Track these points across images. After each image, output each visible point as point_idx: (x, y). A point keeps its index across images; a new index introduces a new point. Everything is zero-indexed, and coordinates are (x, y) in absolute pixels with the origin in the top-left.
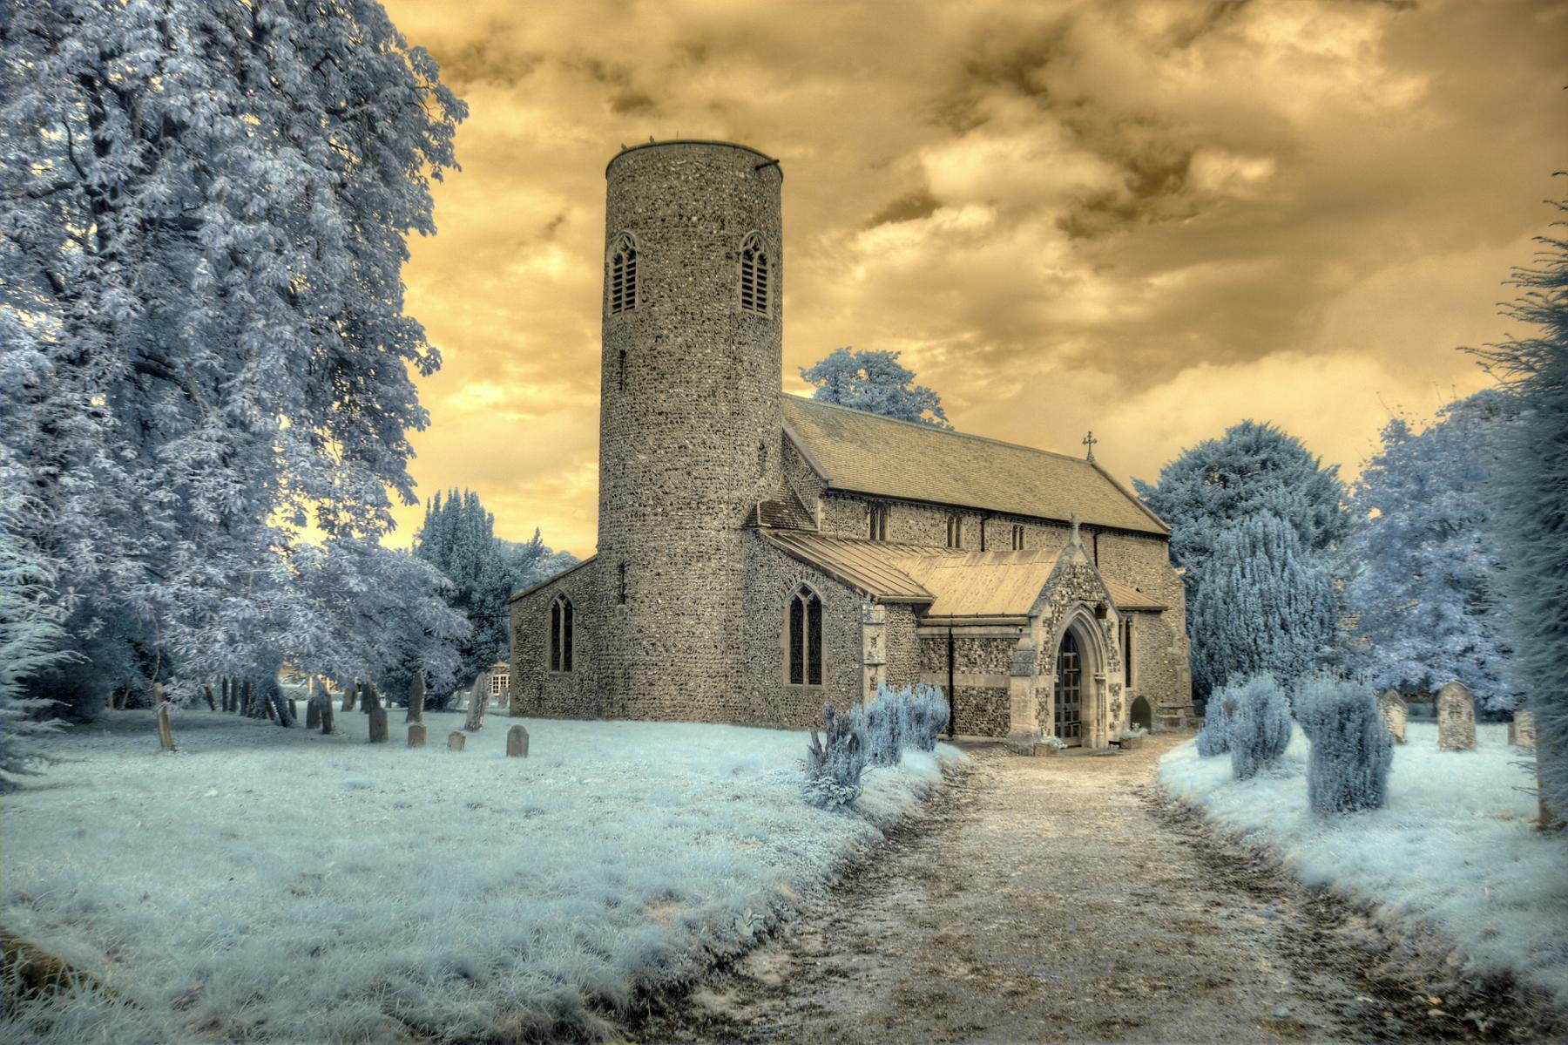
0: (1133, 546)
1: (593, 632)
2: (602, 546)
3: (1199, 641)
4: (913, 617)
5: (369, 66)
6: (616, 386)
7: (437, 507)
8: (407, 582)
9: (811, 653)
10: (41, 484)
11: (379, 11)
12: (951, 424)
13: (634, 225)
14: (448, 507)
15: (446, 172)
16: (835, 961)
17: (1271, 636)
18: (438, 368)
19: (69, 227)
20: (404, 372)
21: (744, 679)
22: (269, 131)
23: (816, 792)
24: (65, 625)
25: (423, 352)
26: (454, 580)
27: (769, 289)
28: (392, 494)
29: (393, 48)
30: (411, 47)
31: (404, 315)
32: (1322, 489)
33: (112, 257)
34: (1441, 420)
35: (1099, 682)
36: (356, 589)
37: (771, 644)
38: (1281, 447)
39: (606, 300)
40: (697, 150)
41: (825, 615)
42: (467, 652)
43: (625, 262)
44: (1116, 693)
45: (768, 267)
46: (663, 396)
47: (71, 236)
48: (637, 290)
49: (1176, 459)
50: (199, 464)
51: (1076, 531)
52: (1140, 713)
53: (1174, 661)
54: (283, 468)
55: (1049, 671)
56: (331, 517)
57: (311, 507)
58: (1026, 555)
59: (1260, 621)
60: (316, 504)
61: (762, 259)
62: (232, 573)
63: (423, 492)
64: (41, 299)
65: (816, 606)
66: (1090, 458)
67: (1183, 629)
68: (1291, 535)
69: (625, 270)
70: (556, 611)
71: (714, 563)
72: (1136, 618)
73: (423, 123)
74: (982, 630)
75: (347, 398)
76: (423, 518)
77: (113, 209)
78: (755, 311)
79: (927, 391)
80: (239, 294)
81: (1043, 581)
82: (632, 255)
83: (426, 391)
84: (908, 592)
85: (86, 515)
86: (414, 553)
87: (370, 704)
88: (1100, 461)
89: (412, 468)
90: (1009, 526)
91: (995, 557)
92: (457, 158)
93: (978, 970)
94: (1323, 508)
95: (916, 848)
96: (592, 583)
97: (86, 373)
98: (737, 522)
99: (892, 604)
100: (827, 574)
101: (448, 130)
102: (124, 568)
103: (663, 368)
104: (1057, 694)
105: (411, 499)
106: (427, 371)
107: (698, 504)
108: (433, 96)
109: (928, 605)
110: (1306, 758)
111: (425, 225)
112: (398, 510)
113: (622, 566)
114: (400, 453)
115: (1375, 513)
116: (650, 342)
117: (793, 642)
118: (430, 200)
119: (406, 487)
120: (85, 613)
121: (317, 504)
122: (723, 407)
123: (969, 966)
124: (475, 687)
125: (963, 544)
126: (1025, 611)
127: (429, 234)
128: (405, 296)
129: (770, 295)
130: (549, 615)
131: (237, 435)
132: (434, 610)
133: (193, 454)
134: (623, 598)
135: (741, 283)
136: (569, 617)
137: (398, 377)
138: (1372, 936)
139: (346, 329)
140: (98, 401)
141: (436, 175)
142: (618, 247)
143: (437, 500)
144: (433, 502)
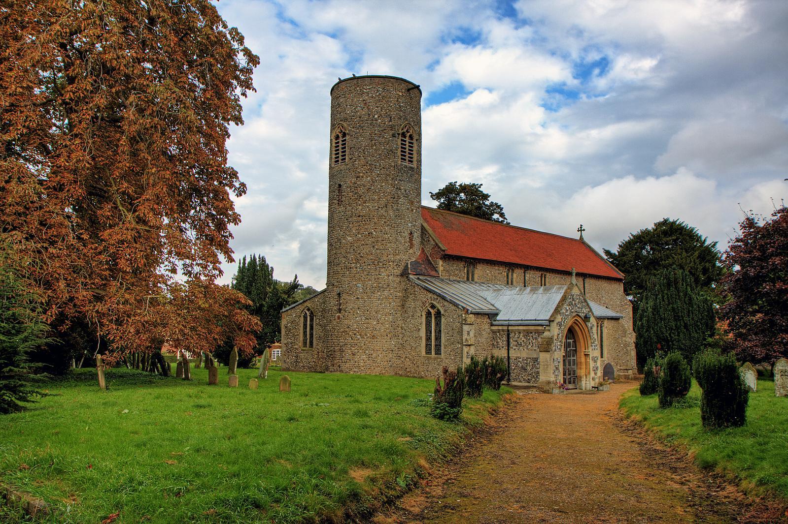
0: (604, 285)
1: (324, 327)
2: (329, 283)
3: (640, 334)
4: (488, 321)
5: (208, 38)
6: (336, 202)
7: (244, 263)
8: (232, 303)
9: (436, 339)
10: (39, 252)
11: (213, 9)
12: (508, 221)
13: (346, 120)
14: (250, 263)
15: (249, 92)
16: (449, 501)
17: (679, 333)
18: (245, 193)
19: (53, 121)
20: (228, 194)
21: (401, 352)
22: (157, 71)
23: (438, 411)
24: (50, 325)
25: (237, 185)
26: (253, 301)
27: (414, 152)
28: (221, 257)
29: (221, 28)
30: (230, 27)
31: (227, 166)
32: (707, 254)
33: (76, 135)
34: (775, 218)
35: (587, 355)
36: (203, 306)
37: (415, 334)
38: (683, 232)
39: (331, 158)
40: (377, 80)
41: (443, 320)
42: (258, 338)
43: (341, 139)
44: (595, 362)
45: (414, 141)
46: (360, 207)
47: (55, 125)
48: (347, 153)
49: (627, 239)
50: (122, 242)
51: (574, 277)
52: (608, 371)
53: (626, 345)
54: (165, 243)
55: (560, 349)
56: (190, 269)
57: (179, 264)
58: (546, 290)
59: (673, 324)
60: (182, 262)
61: (411, 137)
62: (138, 298)
63: (237, 256)
64: (39, 158)
65: (438, 314)
67: (631, 328)
68: (690, 279)
69: (341, 143)
70: (305, 317)
72: (606, 322)
73: (236, 67)
74: (525, 328)
75: (198, 208)
76: (237, 269)
77: (76, 112)
78: (406, 164)
79: (496, 204)
80: (142, 155)
81: (557, 302)
82: (344, 135)
83: (239, 203)
84: (486, 308)
85: (62, 268)
86: (232, 287)
87: (209, 364)
88: (586, 239)
89: (231, 244)
90: (539, 274)
91: (531, 290)
92: (254, 85)
93: (524, 507)
94: (707, 265)
95: (490, 441)
96: (324, 303)
97: (61, 195)
98: (398, 271)
99: (477, 314)
100: (444, 298)
101: (249, 71)
102: (83, 294)
103: (360, 193)
104: (564, 360)
105: (231, 260)
106: (239, 195)
107: (377, 262)
108: (241, 54)
109: (497, 314)
110: (700, 398)
111: (238, 120)
112: (224, 264)
113: (339, 294)
114: (225, 236)
115: (737, 268)
116: (354, 180)
117: (427, 333)
118: (240, 107)
119: (228, 252)
120: (61, 318)
121: (183, 262)
122: (391, 213)
123: (519, 505)
124: (263, 356)
125: (515, 283)
126: (548, 318)
127: (240, 125)
128: (228, 156)
129: (415, 156)
130: (302, 319)
131: (140, 227)
132: (242, 316)
133: (119, 237)
134: (340, 310)
135: (400, 149)
136: (312, 320)
137: (225, 198)
138: (740, 497)
139: (198, 173)
140: (69, 210)
141: (244, 94)
142: (337, 131)
143: (244, 259)
144: (242, 261)
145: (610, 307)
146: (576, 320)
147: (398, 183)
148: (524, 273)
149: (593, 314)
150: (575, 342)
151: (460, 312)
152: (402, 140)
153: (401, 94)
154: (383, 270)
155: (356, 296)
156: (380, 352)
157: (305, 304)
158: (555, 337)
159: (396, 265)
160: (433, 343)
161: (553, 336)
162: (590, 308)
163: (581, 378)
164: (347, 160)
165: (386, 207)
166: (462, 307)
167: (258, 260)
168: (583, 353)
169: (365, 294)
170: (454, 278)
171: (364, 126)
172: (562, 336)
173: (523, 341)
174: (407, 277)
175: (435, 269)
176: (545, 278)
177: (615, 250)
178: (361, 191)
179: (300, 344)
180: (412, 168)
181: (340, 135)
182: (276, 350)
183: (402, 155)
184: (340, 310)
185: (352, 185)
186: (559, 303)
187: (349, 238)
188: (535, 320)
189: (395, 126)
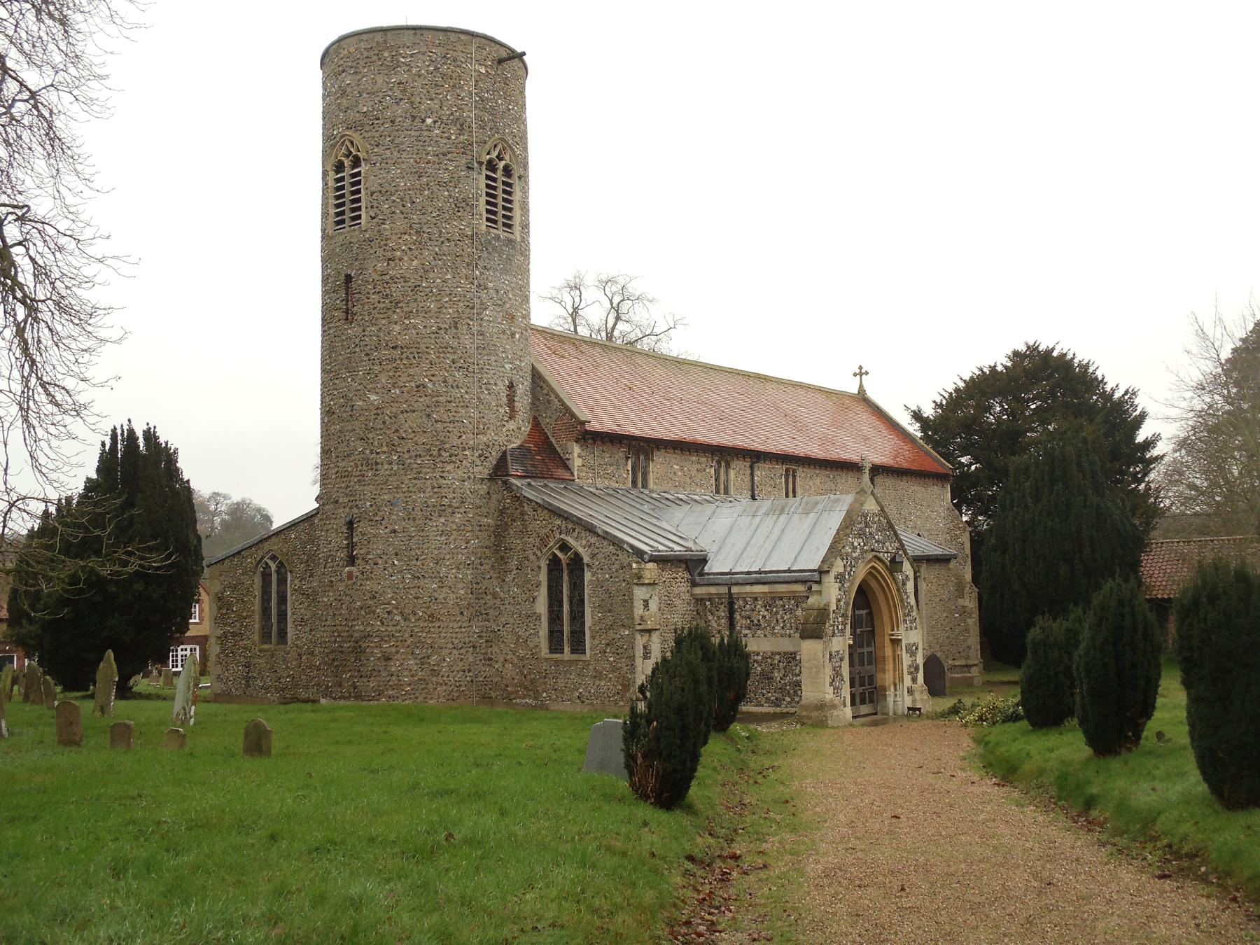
4: (686, 575)
35: (896, 642)
39: (325, 215)
41: (588, 576)
43: (348, 172)
45: (514, 180)
46: (397, 328)
48: (363, 204)
53: (964, 612)
55: (843, 631)
65: (577, 562)
66: (861, 390)
70: (266, 576)
71: (458, 517)
74: (765, 589)
82: (356, 162)
88: (872, 394)
90: (780, 469)
98: (483, 471)
99: (662, 561)
100: (591, 529)
103: (397, 295)
104: (850, 655)
116: (381, 266)
117: (550, 606)
129: (517, 214)
130: (258, 580)
135: (484, 199)
145: (926, 534)
146: (873, 567)
147: (482, 274)
148: (752, 467)
149: (906, 553)
150: (870, 614)
151: (623, 558)
152: (488, 177)
153: (483, 71)
154: (450, 467)
155: (390, 528)
156: (447, 651)
157: (266, 546)
158: (833, 607)
159: (480, 456)
160: (566, 629)
161: (828, 605)
162: (900, 541)
163: (885, 690)
164: (363, 220)
165: (456, 328)
166: (632, 546)
167: (141, 442)
168: (887, 638)
169: (411, 522)
170: (606, 482)
171: (402, 143)
172: (847, 604)
173: (764, 617)
174: (505, 482)
175: (564, 464)
176: (794, 477)
177: (929, 412)
178: (396, 290)
179: (256, 637)
180: (510, 241)
181: (347, 162)
182: (188, 647)
183: (488, 211)
184: (352, 560)
185: (376, 277)
186: (838, 533)
187: (373, 397)
188: (789, 571)
189: (471, 144)
